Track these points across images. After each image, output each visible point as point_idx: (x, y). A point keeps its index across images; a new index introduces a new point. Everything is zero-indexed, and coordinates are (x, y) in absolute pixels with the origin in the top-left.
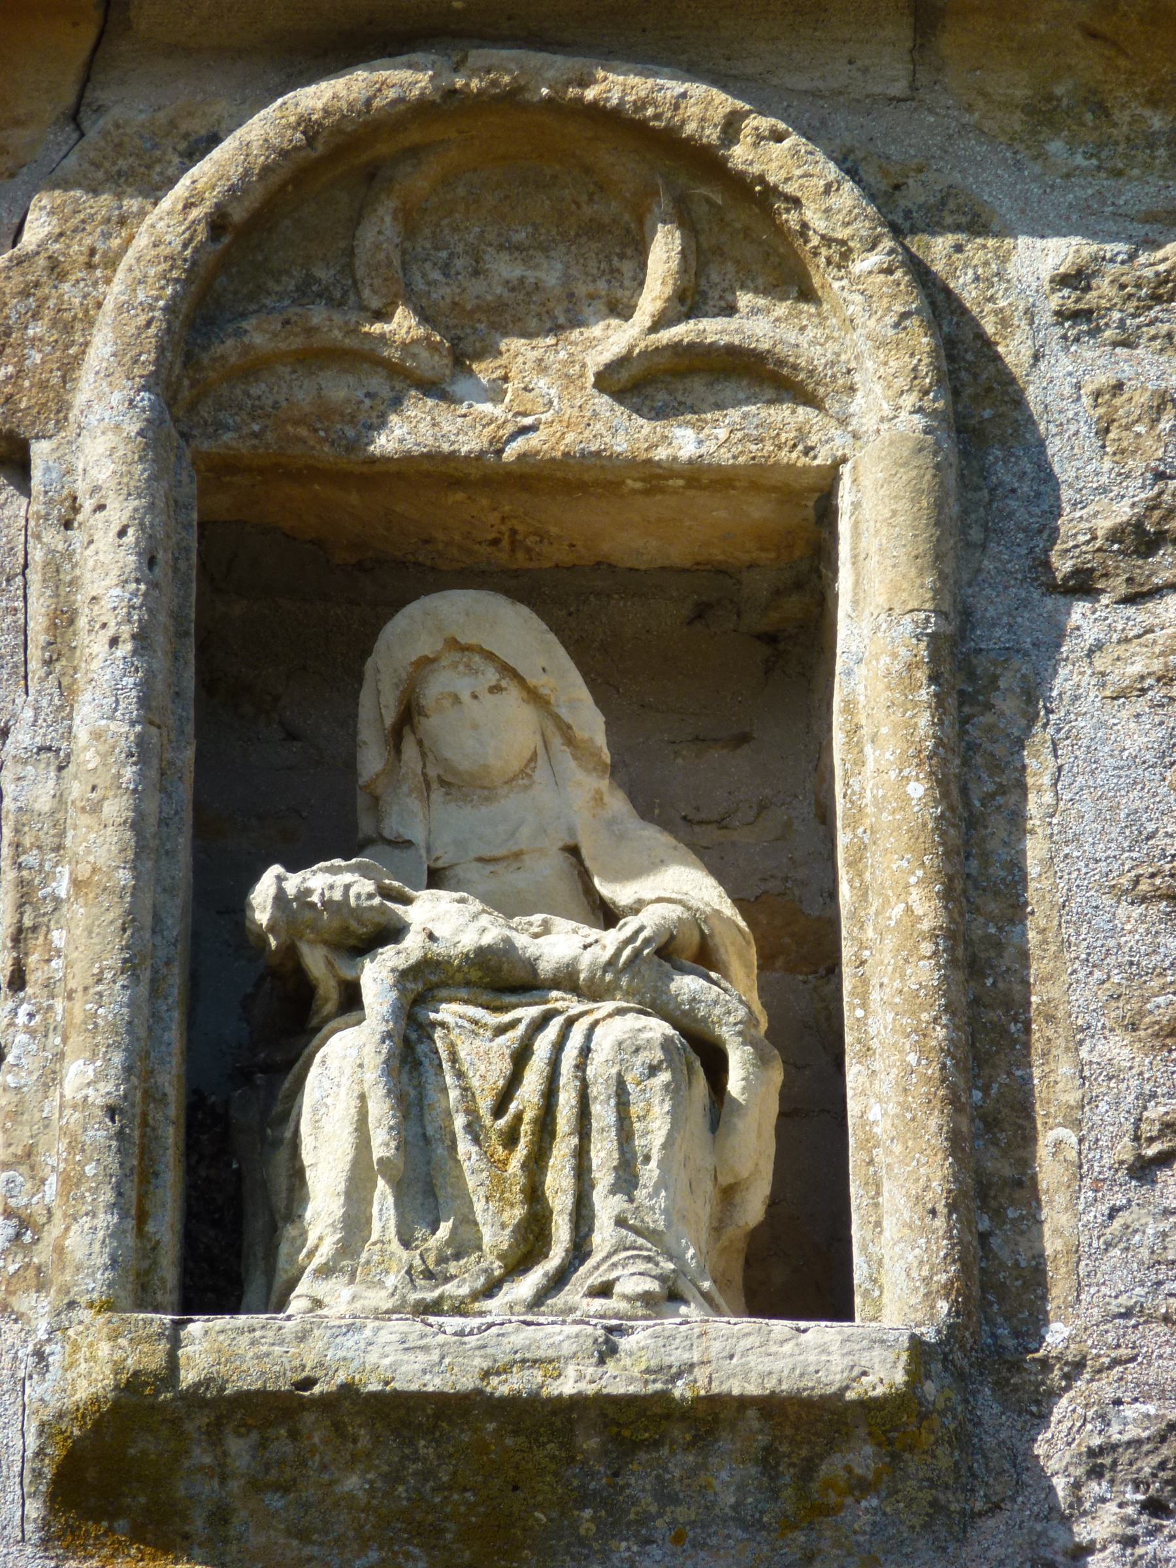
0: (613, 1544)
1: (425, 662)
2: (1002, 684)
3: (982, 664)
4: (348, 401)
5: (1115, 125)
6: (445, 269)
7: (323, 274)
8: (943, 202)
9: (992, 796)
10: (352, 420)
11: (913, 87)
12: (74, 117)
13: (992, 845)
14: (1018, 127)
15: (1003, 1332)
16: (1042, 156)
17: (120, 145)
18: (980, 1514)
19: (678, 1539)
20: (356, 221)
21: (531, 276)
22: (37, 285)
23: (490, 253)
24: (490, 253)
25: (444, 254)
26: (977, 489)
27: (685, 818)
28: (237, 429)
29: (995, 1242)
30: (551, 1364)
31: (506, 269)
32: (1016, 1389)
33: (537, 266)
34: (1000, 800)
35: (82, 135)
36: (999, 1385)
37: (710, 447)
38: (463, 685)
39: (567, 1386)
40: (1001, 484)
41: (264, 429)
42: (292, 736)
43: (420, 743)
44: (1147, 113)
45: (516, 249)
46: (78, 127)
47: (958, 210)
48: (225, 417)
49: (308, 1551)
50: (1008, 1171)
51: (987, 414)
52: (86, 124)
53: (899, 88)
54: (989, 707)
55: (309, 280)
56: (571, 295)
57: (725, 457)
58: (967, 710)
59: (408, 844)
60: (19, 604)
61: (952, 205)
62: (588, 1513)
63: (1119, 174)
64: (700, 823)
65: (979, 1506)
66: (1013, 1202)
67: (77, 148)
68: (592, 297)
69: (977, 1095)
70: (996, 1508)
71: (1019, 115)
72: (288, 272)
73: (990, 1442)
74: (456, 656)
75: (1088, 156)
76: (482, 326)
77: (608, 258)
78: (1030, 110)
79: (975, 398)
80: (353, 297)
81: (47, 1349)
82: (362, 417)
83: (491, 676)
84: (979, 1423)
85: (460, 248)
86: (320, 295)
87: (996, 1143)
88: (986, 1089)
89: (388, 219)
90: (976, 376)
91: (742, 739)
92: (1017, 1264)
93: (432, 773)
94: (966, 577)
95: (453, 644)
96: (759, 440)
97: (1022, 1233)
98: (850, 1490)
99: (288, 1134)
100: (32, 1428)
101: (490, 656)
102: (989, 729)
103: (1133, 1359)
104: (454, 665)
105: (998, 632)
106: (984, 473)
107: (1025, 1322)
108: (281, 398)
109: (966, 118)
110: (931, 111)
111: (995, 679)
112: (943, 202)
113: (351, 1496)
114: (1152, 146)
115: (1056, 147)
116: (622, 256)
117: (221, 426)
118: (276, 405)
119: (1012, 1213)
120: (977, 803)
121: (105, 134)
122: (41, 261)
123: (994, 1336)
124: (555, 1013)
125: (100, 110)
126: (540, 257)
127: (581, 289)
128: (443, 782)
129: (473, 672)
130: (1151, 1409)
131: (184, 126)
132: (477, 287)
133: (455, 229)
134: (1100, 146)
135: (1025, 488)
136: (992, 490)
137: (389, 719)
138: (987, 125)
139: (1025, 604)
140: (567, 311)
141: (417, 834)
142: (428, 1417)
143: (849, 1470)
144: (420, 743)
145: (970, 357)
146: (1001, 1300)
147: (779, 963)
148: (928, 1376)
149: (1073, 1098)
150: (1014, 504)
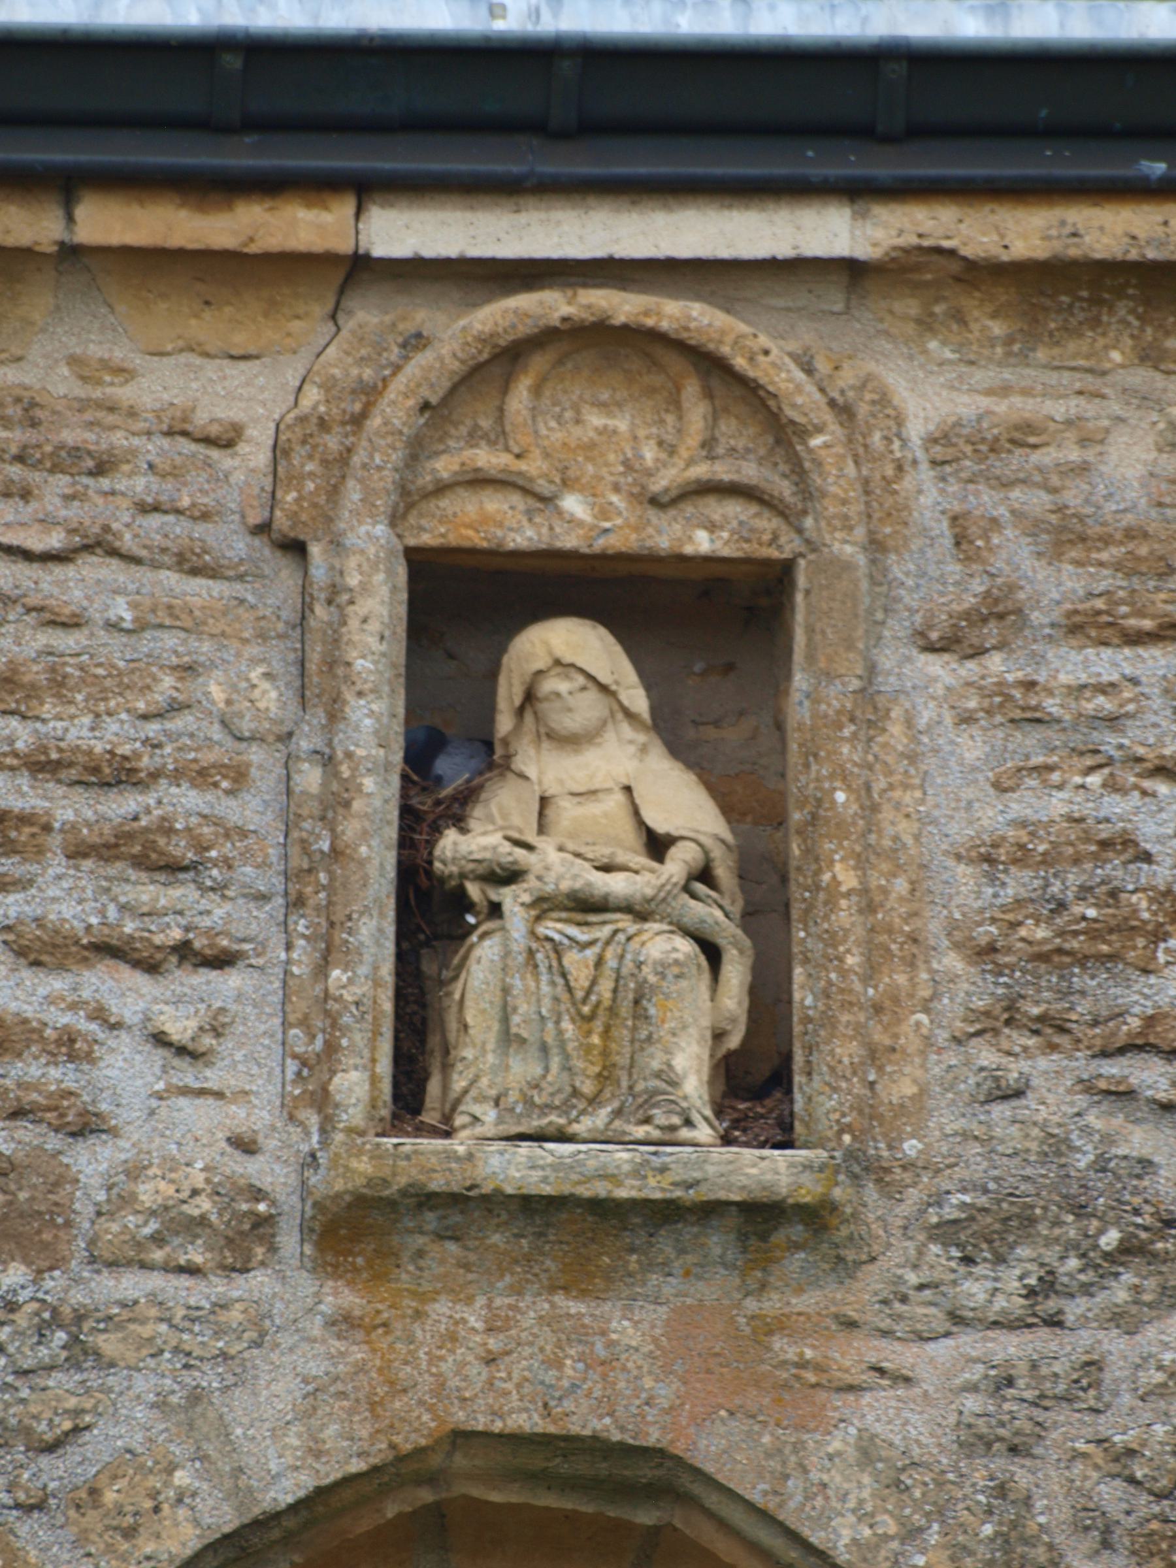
0: (649, 1275)
1: (540, 672)
2: (893, 714)
3: (881, 701)
4: (498, 511)
5: (971, 332)
6: (559, 419)
7: (485, 423)
8: (864, 385)
9: (885, 791)
10: (500, 525)
11: (848, 308)
12: (333, 317)
13: (885, 825)
14: (911, 332)
15: (882, 1145)
16: (925, 352)
17: (362, 339)
18: (864, 1263)
19: (687, 1274)
20: (505, 390)
21: (611, 423)
22: (311, 435)
23: (586, 409)
24: (586, 409)
25: (557, 409)
26: (881, 584)
27: (693, 721)
28: (431, 531)
29: (878, 1087)
30: (613, 1178)
31: (596, 420)
32: (888, 1184)
33: (614, 417)
34: (890, 794)
35: (339, 329)
36: (879, 1181)
37: (719, 544)
38: (563, 687)
39: (622, 1193)
40: (895, 579)
41: (448, 530)
42: (451, 656)
43: (535, 713)
44: (990, 323)
45: (602, 406)
46: (336, 324)
47: (873, 391)
48: (423, 522)
49: (470, 1277)
50: (887, 1042)
51: (888, 530)
52: (341, 322)
53: (838, 307)
54: (884, 730)
55: (476, 427)
56: (635, 438)
57: (726, 552)
58: (872, 732)
59: (526, 778)
60: (298, 646)
61: (870, 386)
62: (634, 1257)
63: (972, 363)
64: (703, 724)
65: (864, 1257)
66: (890, 1062)
67: (335, 342)
68: (648, 438)
69: (871, 991)
70: (873, 1259)
71: (912, 325)
72: (462, 423)
73: (871, 1217)
74: (559, 670)
75: (953, 351)
76: (580, 459)
77: (658, 413)
78: (919, 322)
79: (880, 520)
80: (502, 440)
81: (319, 1154)
82: (507, 523)
83: (581, 680)
84: (865, 1206)
85: (567, 405)
86: (482, 438)
87: (880, 1022)
88: (876, 987)
89: (525, 393)
90: (881, 505)
91: (729, 668)
92: (891, 1103)
93: (543, 730)
94: (872, 642)
95: (558, 662)
96: (748, 541)
97: (894, 1082)
98: (788, 1249)
99: (456, 960)
100: (309, 1203)
101: (582, 671)
102: (885, 745)
103: (956, 1165)
104: (558, 675)
105: (892, 679)
106: (885, 571)
107: (893, 1139)
108: (458, 510)
109: (880, 326)
110: (858, 321)
111: (888, 710)
112: (864, 385)
113: (496, 1245)
114: (993, 346)
115: (933, 345)
116: (667, 411)
117: (421, 529)
118: (455, 515)
119: (889, 1069)
120: (876, 796)
121: (353, 332)
122: (314, 420)
123: (876, 1148)
124: (623, 930)
125: (350, 313)
126: (615, 409)
127: (641, 433)
128: (548, 735)
129: (568, 677)
130: (967, 1199)
131: (401, 327)
132: (577, 431)
133: (565, 392)
134: (962, 345)
135: (910, 582)
136: (890, 583)
137: (518, 701)
138: (893, 331)
139: (909, 659)
140: (633, 448)
141: (531, 771)
142: (566, 1356)
143: (788, 1238)
144: (535, 713)
145: (878, 491)
146: (881, 1125)
147: (749, 819)
148: (837, 1184)
149: (926, 993)
150: (902, 592)
